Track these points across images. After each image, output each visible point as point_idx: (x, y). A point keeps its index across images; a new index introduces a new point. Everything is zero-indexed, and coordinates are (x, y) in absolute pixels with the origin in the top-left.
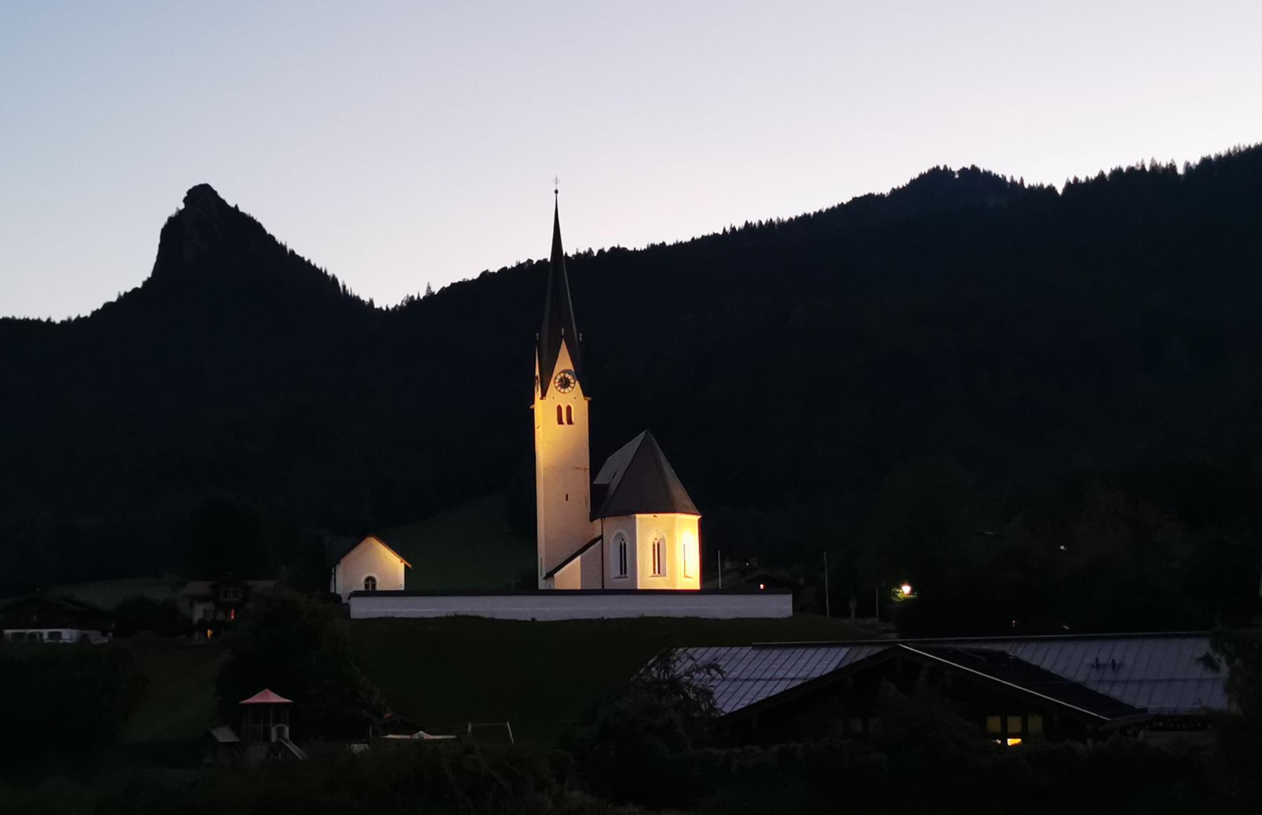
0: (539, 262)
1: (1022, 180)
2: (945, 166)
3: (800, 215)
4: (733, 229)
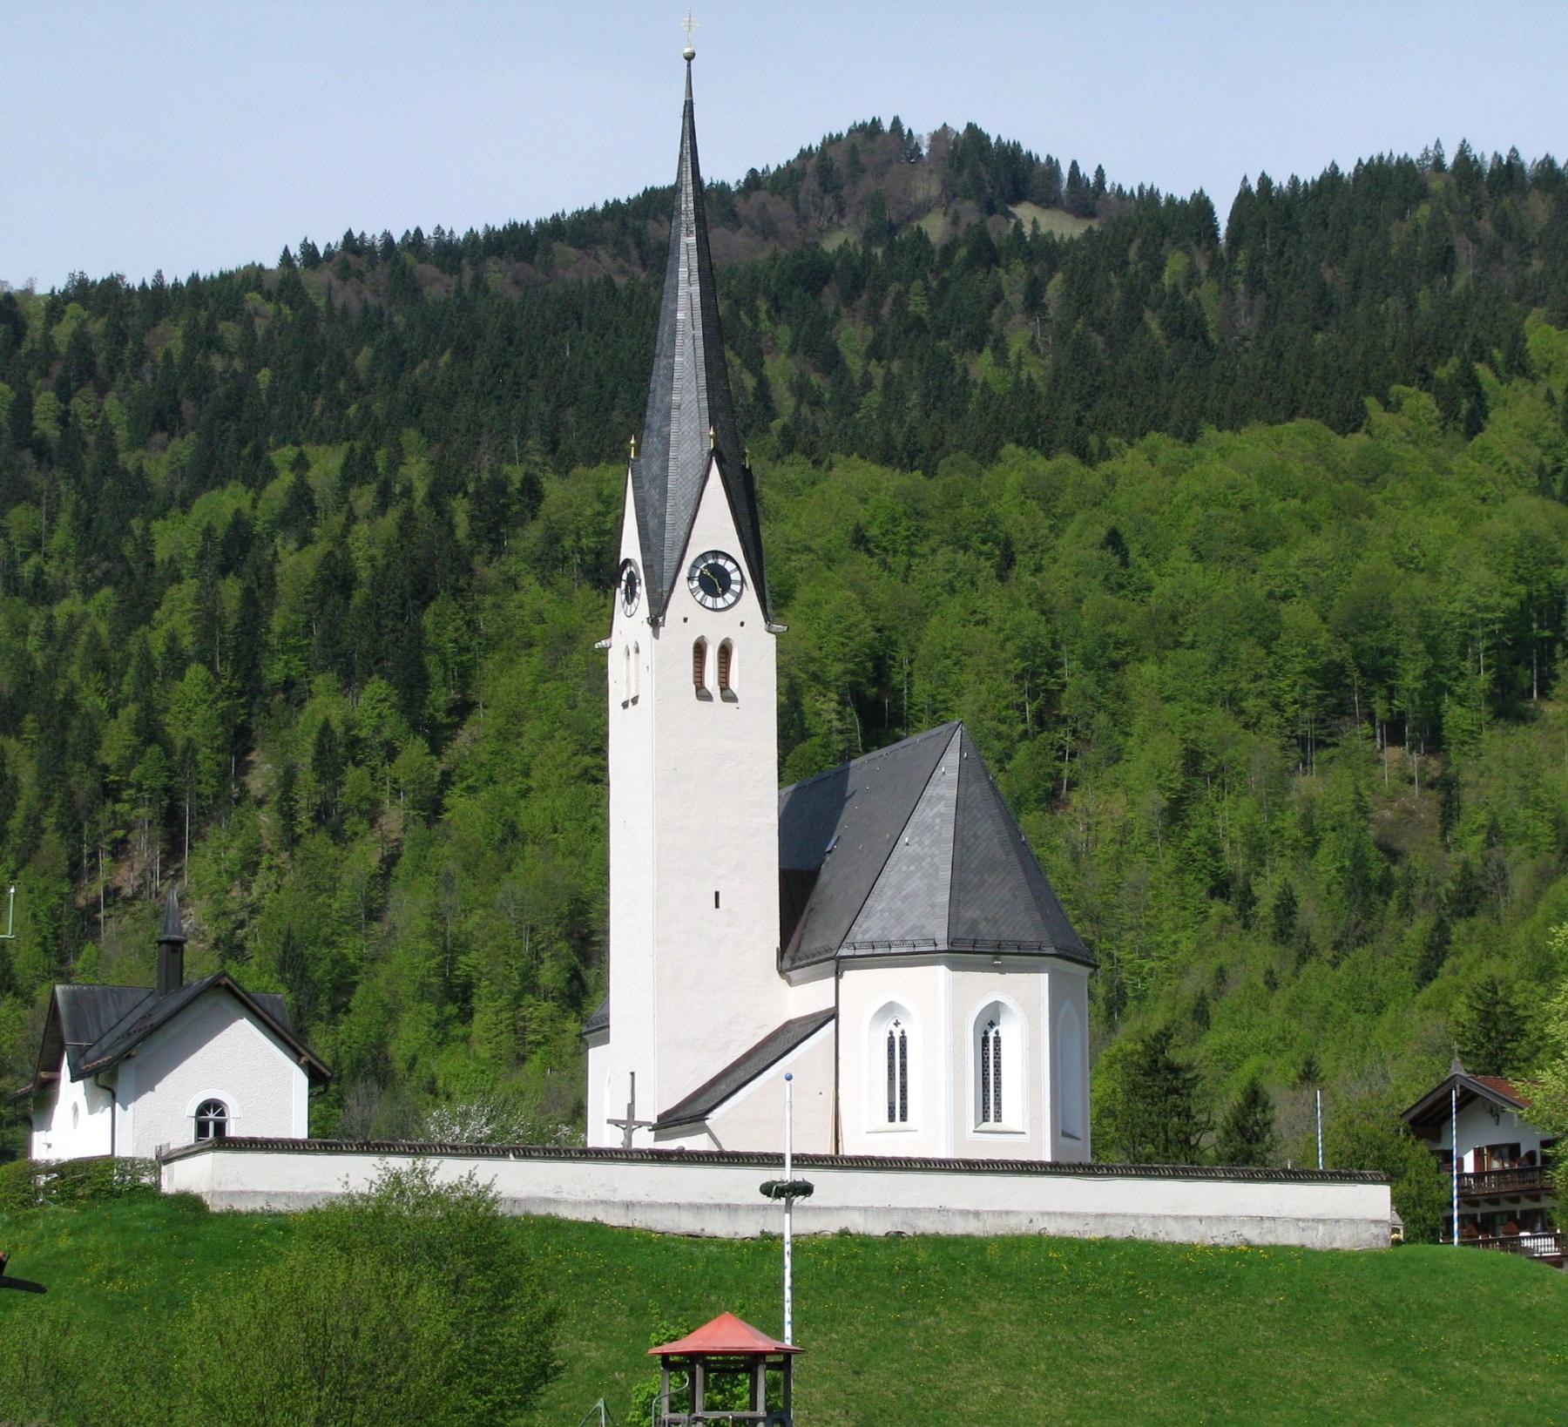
0: (103, 281)
1: (1100, 173)
2: (896, 123)
3: (499, 227)
4: (309, 250)
